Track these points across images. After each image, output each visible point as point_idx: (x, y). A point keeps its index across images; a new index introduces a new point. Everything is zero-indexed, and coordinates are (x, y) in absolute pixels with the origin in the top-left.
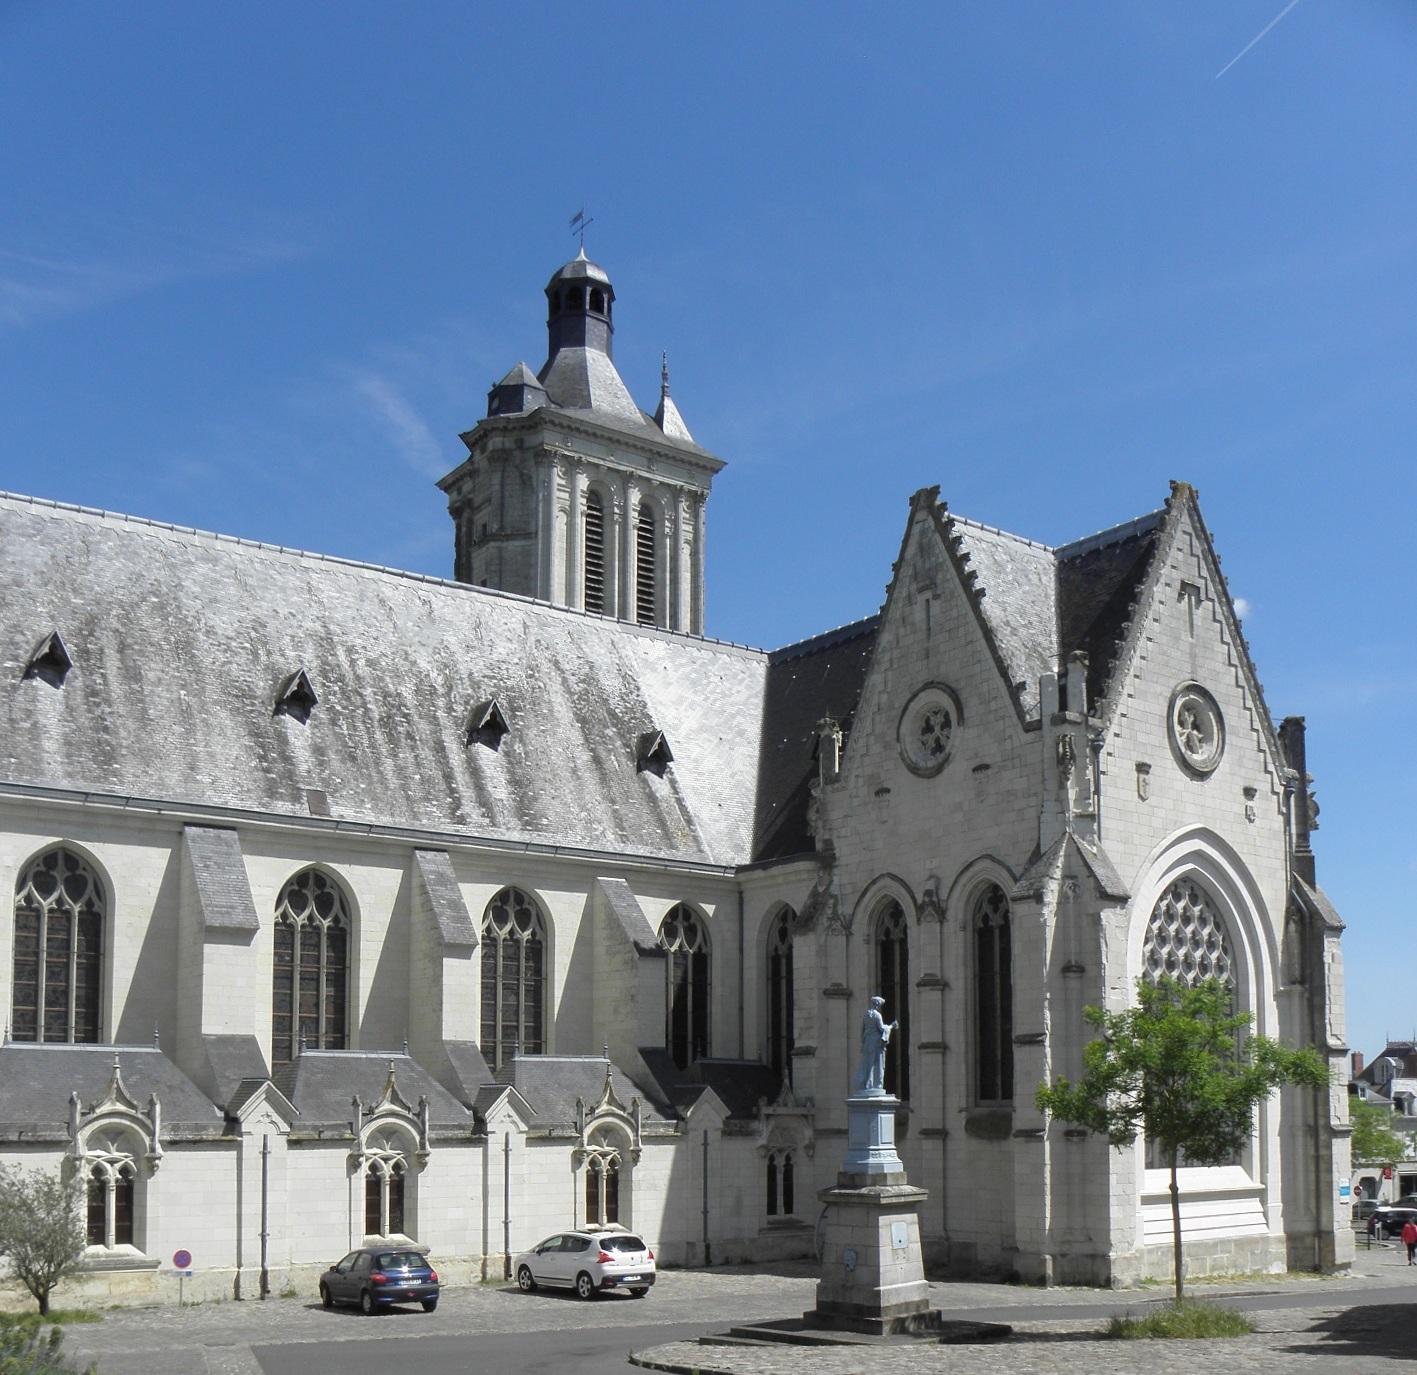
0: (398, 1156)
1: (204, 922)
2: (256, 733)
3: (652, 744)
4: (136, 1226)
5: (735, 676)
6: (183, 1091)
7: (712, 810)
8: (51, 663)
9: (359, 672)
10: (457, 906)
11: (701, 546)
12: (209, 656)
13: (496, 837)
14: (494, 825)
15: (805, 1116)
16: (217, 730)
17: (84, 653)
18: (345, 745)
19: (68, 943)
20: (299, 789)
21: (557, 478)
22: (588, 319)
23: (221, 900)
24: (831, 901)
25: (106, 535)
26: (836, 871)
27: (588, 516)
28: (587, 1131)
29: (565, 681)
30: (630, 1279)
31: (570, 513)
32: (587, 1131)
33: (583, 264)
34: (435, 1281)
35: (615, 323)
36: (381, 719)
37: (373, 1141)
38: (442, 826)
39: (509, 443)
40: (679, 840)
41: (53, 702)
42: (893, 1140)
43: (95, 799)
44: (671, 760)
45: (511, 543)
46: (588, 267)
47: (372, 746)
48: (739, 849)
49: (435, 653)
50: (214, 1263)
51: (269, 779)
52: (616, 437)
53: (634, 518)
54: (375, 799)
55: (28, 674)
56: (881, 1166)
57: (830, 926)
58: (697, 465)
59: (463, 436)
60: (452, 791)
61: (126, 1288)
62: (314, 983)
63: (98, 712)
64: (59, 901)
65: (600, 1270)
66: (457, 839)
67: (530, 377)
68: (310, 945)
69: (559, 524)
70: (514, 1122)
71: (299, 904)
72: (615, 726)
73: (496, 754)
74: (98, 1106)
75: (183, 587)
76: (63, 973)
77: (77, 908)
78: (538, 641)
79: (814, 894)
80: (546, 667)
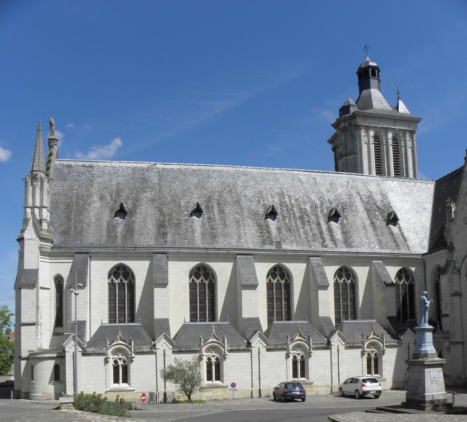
0: (302, 353)
1: (317, 284)
2: (259, 225)
3: (391, 215)
4: (221, 376)
5: (423, 190)
6: (235, 335)
7: (414, 236)
8: (198, 211)
9: (292, 203)
10: (323, 274)
11: (415, 148)
12: (245, 203)
13: (337, 251)
14: (337, 247)
15: (446, 338)
16: (247, 226)
17: (207, 207)
18: (288, 226)
19: (205, 292)
20: (272, 241)
21: (363, 133)
22: (371, 80)
23: (248, 277)
24: (453, 263)
25: (214, 172)
26: (454, 252)
27: (375, 144)
28: (366, 344)
29: (361, 198)
30: (372, 392)
31: (368, 144)
32: (366, 344)
33: (368, 62)
34: (304, 392)
35: (380, 79)
36: (299, 217)
37: (294, 349)
38: (319, 249)
39: (346, 124)
40: (401, 247)
41: (198, 222)
42: (432, 341)
43: (209, 249)
44: (398, 220)
45: (349, 157)
46: (369, 62)
47: (296, 226)
48: (423, 248)
49: (317, 194)
50: (245, 387)
51: (263, 239)
52: (382, 116)
53: (390, 142)
54: (297, 242)
55: (191, 215)
56: (426, 351)
57: (453, 271)
58: (411, 121)
59: (332, 125)
60: (322, 237)
61: (218, 394)
62: (272, 301)
63: (211, 224)
64: (202, 281)
65: (362, 389)
66: (323, 252)
67: (352, 102)
68: (278, 289)
69: (365, 148)
70: (340, 342)
71: (340, 277)
72: (379, 211)
73: (338, 224)
74: (208, 340)
75: (237, 184)
76: (204, 302)
77: (207, 282)
78: (352, 186)
79: (447, 261)
80: (355, 194)
